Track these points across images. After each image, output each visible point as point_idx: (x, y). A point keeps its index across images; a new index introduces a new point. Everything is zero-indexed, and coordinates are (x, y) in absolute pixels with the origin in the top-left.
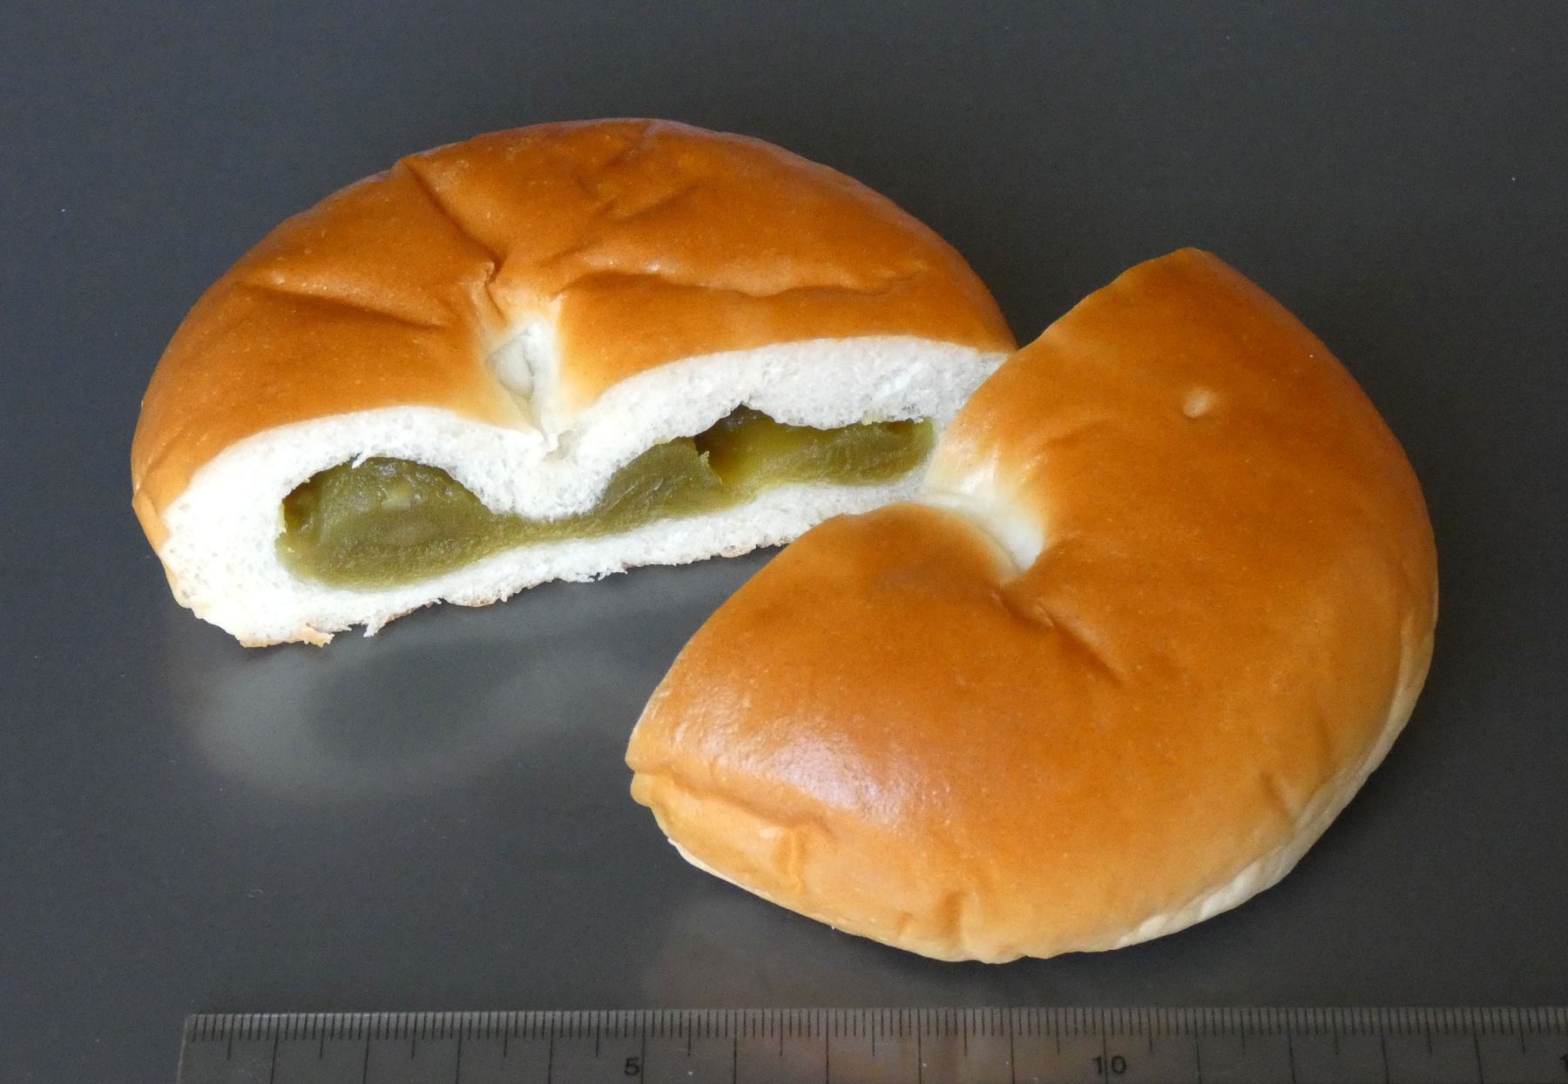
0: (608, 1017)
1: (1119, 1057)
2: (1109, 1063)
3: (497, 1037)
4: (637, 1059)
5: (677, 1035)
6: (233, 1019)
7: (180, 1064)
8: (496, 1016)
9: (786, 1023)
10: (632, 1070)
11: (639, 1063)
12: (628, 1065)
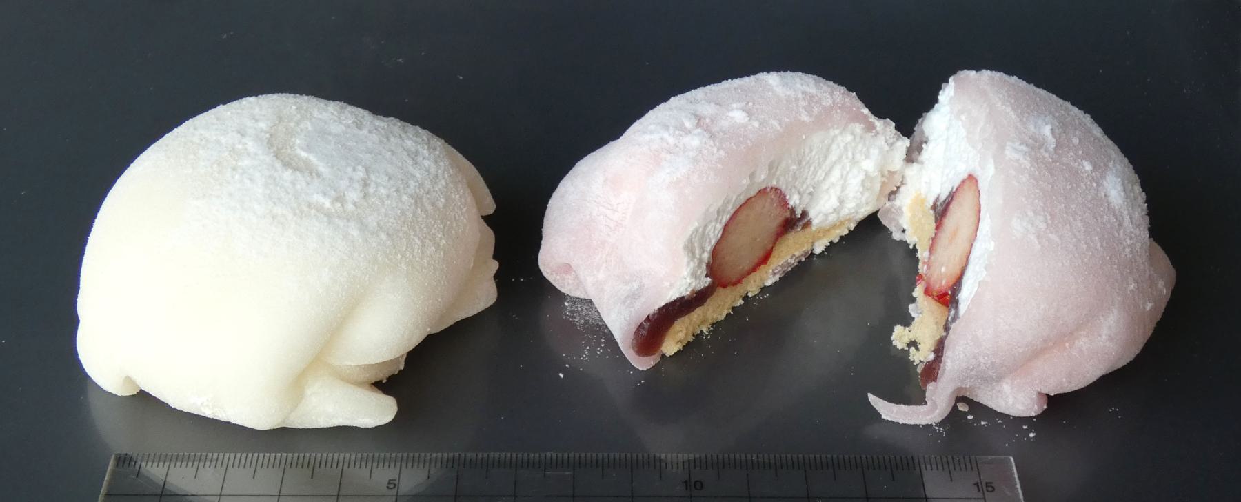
0: (207, 456)
1: (697, 481)
2: (693, 483)
3: (649, 467)
4: (395, 480)
5: (237, 466)
6: (264, 456)
7: (106, 479)
8: (458, 456)
9: (318, 461)
10: (392, 486)
11: (396, 482)
12: (389, 483)
